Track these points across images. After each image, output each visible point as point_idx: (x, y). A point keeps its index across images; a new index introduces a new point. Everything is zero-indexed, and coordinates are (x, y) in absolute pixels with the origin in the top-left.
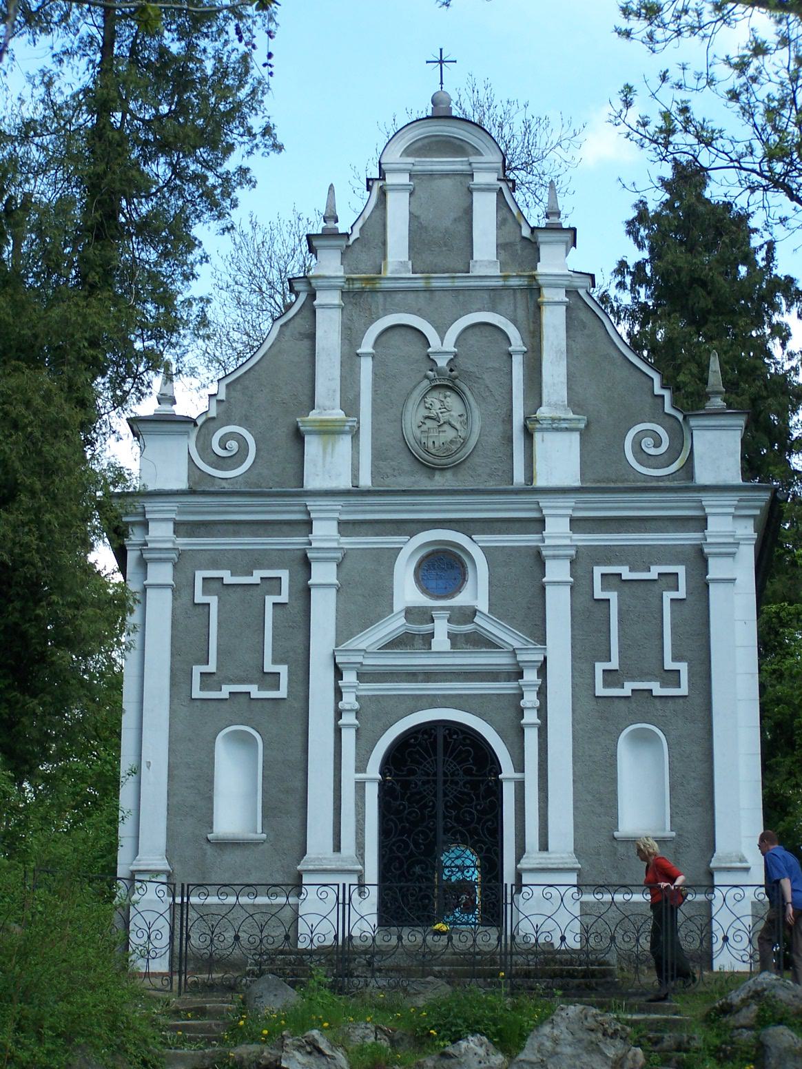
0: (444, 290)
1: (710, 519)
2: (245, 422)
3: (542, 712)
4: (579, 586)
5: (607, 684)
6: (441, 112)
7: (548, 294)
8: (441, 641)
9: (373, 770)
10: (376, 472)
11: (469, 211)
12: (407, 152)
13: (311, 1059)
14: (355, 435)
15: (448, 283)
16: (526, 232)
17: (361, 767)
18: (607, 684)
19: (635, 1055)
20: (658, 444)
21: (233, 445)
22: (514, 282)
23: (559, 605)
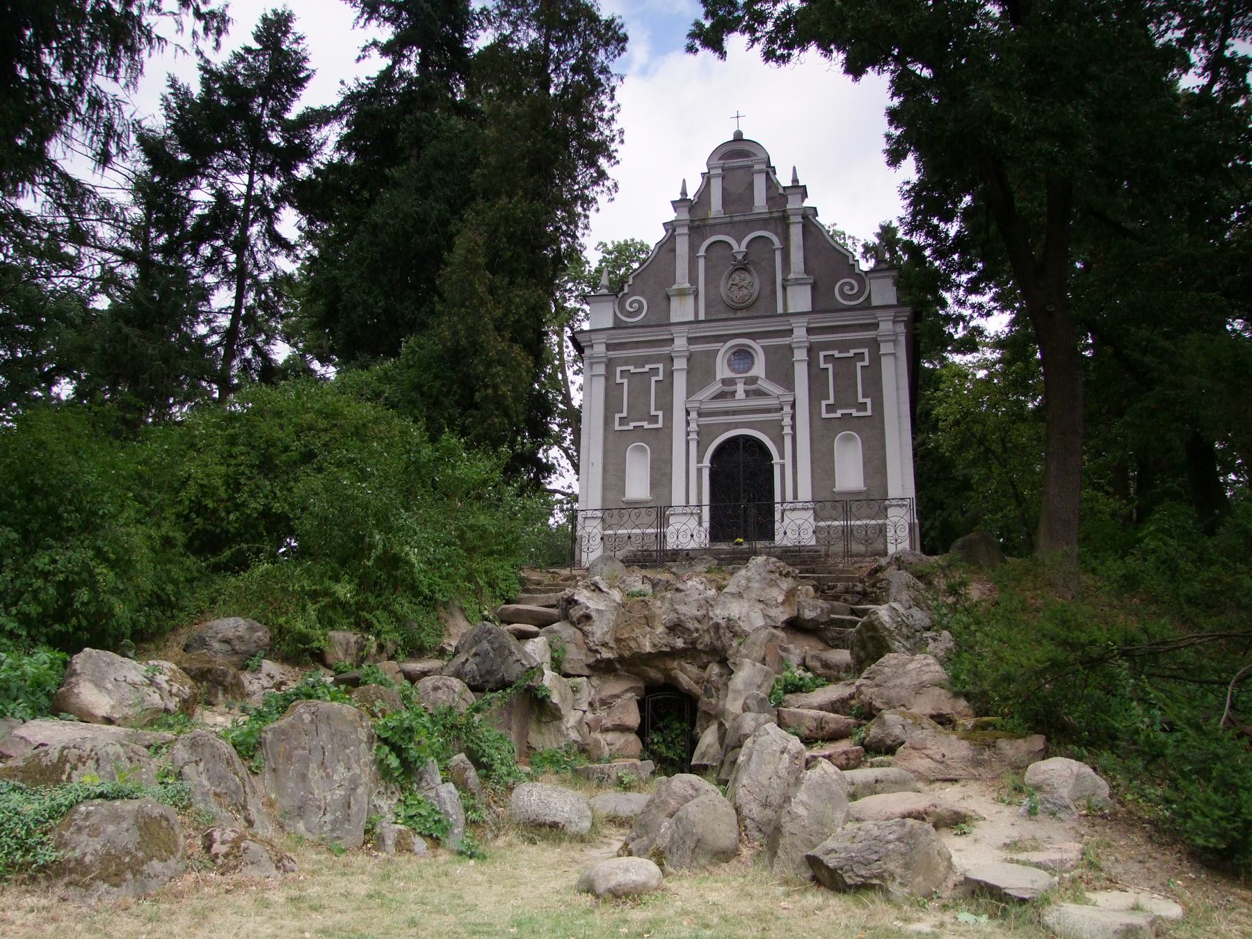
0: (740, 222)
1: (881, 324)
2: (642, 294)
3: (793, 427)
4: (812, 363)
5: (828, 412)
6: (738, 137)
7: (793, 219)
8: (740, 394)
9: (707, 462)
10: (706, 313)
11: (751, 185)
12: (720, 158)
13: (595, 594)
14: (696, 297)
15: (742, 218)
16: (781, 191)
17: (700, 460)
18: (828, 412)
19: (807, 590)
20: (852, 288)
21: (636, 305)
22: (776, 215)
23: (801, 374)
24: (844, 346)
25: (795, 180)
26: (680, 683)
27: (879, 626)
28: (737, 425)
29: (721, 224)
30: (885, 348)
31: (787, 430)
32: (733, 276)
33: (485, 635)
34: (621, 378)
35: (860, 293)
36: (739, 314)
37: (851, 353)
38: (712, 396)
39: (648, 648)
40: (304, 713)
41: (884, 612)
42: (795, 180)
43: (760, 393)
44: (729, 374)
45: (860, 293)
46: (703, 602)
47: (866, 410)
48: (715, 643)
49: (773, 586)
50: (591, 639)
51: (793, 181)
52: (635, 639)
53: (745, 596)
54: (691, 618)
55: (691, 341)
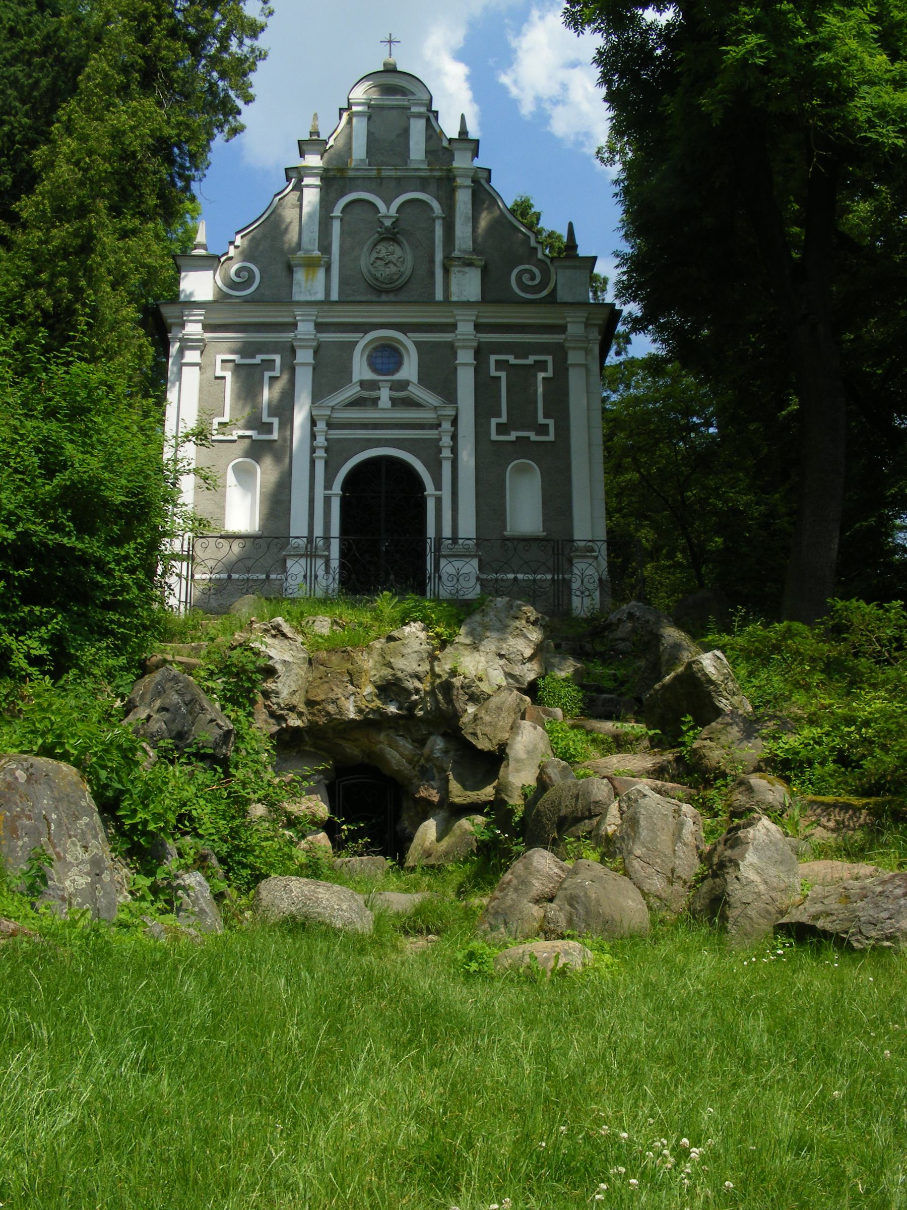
0: (390, 178)
4: (480, 369)
5: (498, 433)
7: (459, 181)
9: (337, 489)
10: (341, 292)
11: (406, 132)
15: (393, 173)
16: (445, 144)
17: (328, 485)
18: (498, 433)
20: (533, 278)
23: (466, 381)
27: (703, 678)
28: (378, 443)
29: (364, 178)
30: (574, 357)
31: (446, 453)
32: (379, 247)
33: (170, 684)
35: (543, 285)
36: (384, 298)
37: (531, 360)
38: (347, 401)
39: (352, 714)
40: (17, 768)
41: (708, 661)
42: (463, 132)
43: (410, 403)
44: (369, 375)
45: (543, 285)
47: (547, 434)
50: (274, 700)
51: (460, 134)
52: (335, 702)
55: (320, 327)
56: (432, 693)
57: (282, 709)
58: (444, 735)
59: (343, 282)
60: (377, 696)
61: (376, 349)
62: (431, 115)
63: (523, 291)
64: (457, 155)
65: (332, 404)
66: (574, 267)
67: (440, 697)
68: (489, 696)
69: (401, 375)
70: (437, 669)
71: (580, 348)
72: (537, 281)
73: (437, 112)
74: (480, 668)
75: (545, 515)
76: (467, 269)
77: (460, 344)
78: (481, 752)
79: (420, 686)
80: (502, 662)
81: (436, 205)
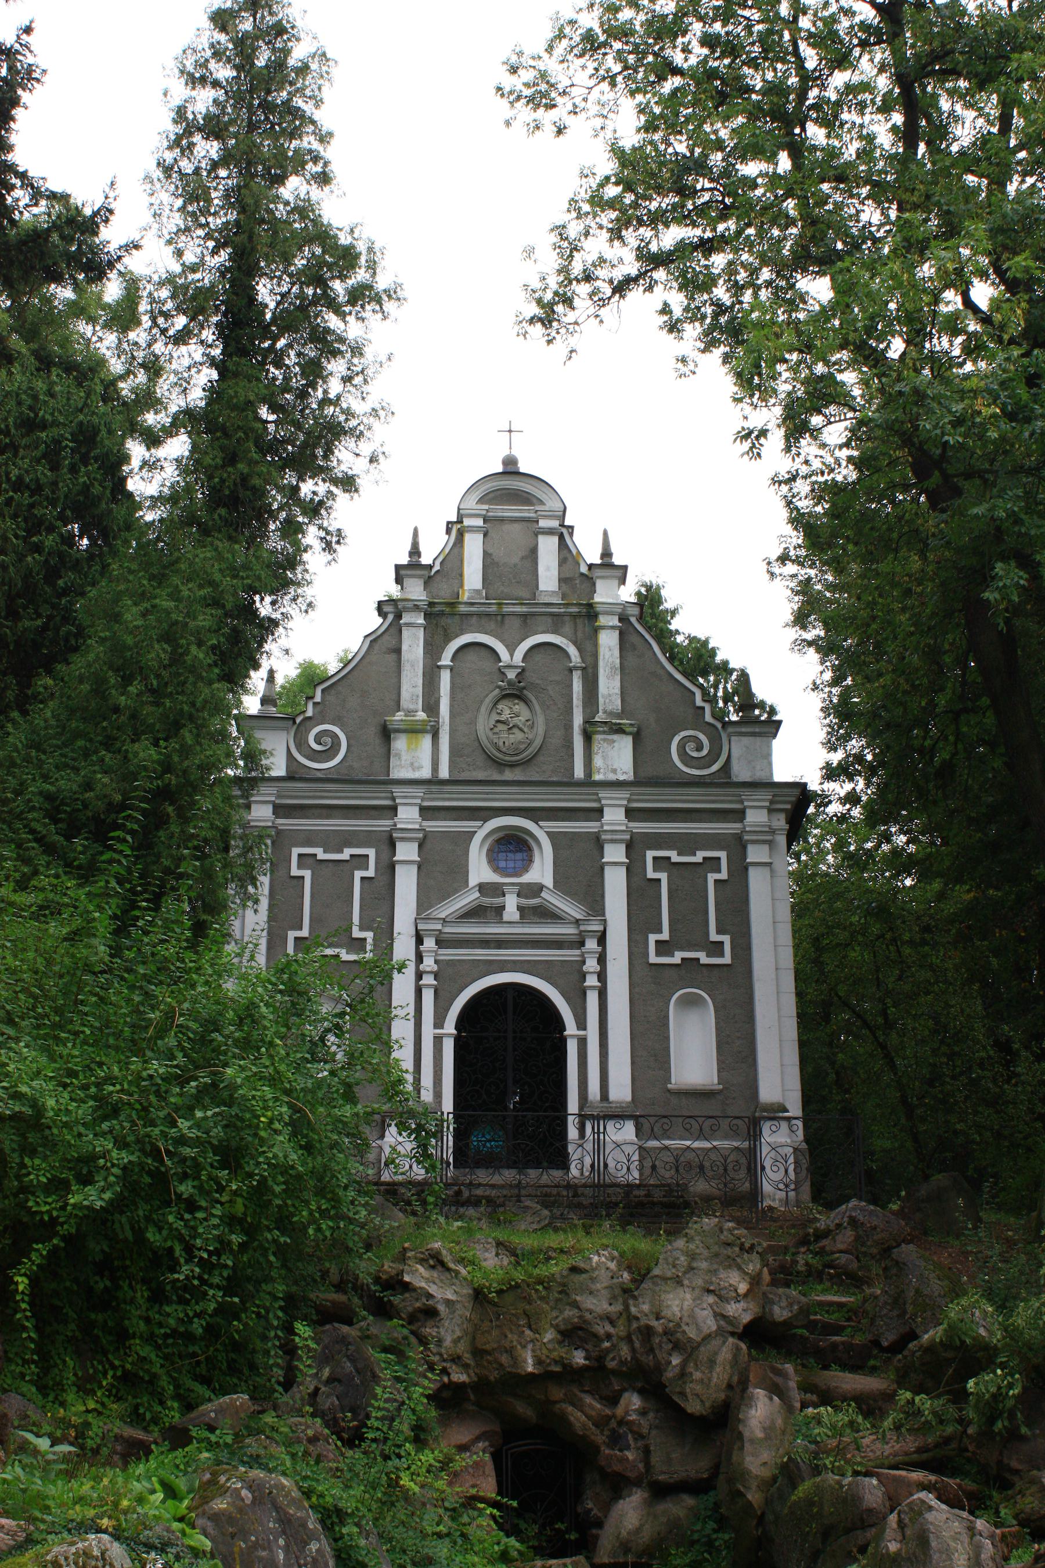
3: (602, 976)
4: (633, 868)
5: (658, 953)
6: (510, 468)
7: (603, 620)
9: (450, 1027)
11: (534, 551)
12: (481, 501)
16: (584, 569)
17: (439, 1023)
18: (658, 953)
20: (699, 748)
24: (687, 844)
25: (606, 554)
26: (570, 1424)
29: (479, 615)
30: (755, 854)
31: (592, 981)
32: (500, 707)
34: (299, 867)
36: (508, 775)
37: (699, 857)
42: (606, 554)
43: (546, 914)
44: (487, 875)
46: (617, 1291)
48: (643, 1359)
49: (730, 1267)
53: (686, 1282)
54: (601, 1318)
55: (426, 812)
56: (629, 1339)
57: (444, 1360)
58: (641, 1392)
59: (455, 752)
60: (560, 1343)
61: (498, 841)
62: (564, 531)
63: (686, 765)
64: (600, 585)
65: (443, 915)
66: (753, 734)
67: (637, 1345)
68: (699, 1344)
69: (532, 876)
70: (633, 1309)
71: (764, 842)
72: (705, 752)
73: (572, 527)
74: (685, 1307)
75: (720, 1062)
76: (615, 737)
77: (608, 837)
78: (691, 1416)
79: (611, 1330)
80: (711, 1299)
81: (572, 651)
